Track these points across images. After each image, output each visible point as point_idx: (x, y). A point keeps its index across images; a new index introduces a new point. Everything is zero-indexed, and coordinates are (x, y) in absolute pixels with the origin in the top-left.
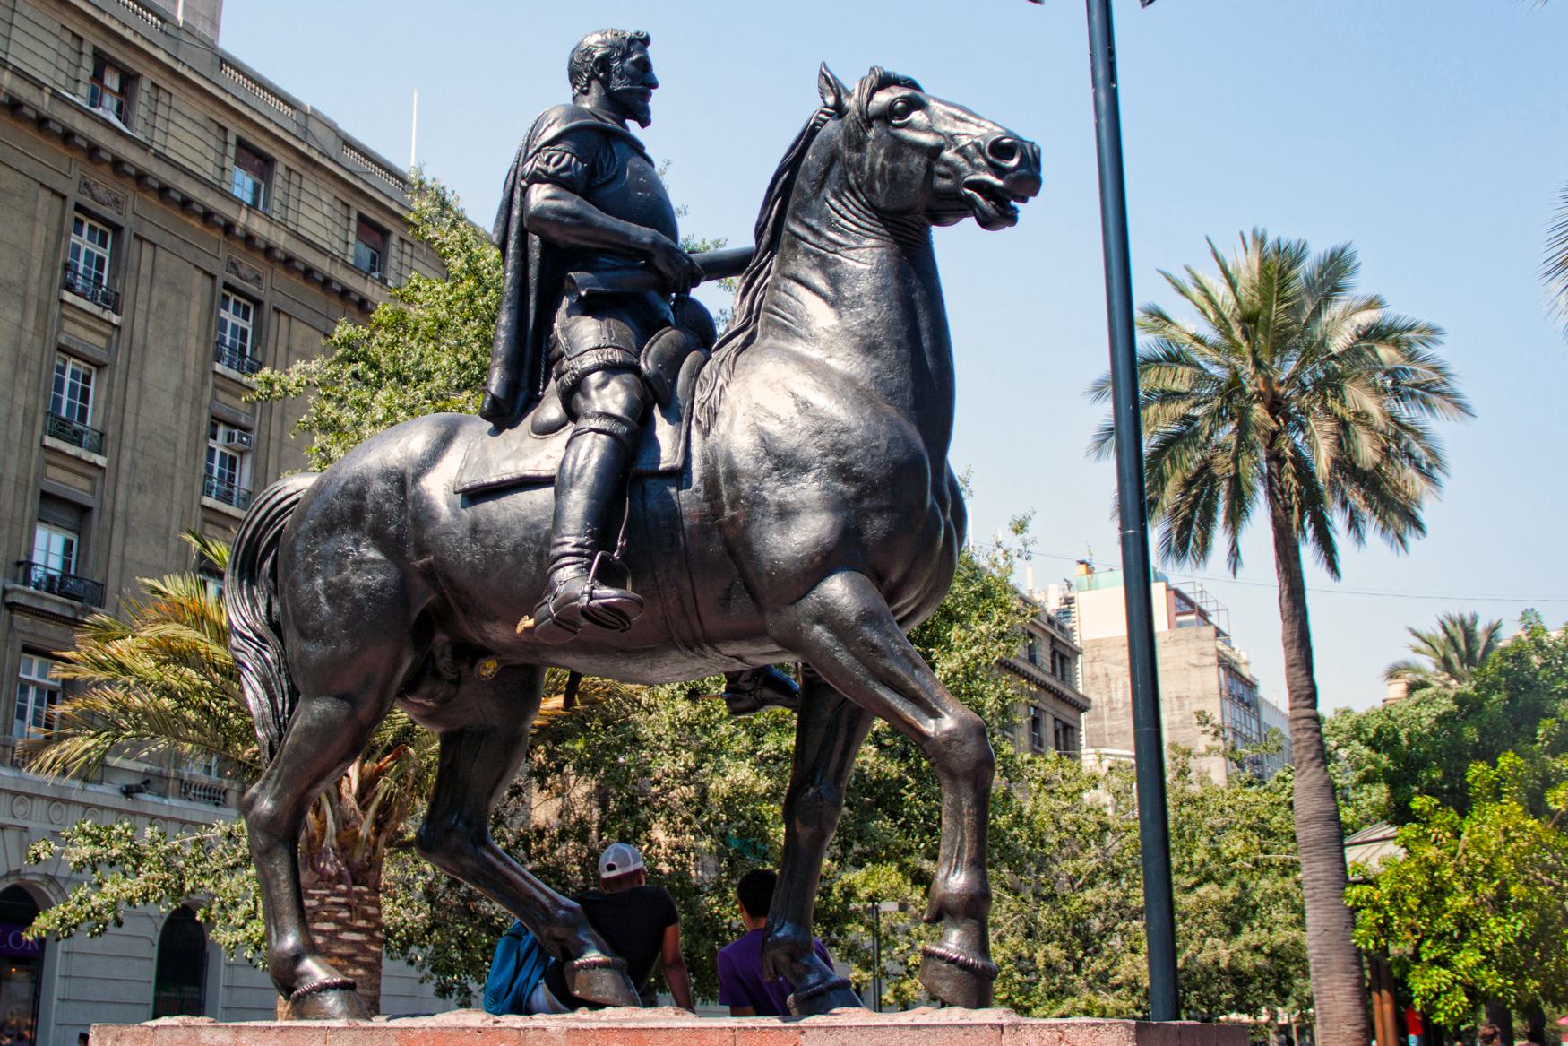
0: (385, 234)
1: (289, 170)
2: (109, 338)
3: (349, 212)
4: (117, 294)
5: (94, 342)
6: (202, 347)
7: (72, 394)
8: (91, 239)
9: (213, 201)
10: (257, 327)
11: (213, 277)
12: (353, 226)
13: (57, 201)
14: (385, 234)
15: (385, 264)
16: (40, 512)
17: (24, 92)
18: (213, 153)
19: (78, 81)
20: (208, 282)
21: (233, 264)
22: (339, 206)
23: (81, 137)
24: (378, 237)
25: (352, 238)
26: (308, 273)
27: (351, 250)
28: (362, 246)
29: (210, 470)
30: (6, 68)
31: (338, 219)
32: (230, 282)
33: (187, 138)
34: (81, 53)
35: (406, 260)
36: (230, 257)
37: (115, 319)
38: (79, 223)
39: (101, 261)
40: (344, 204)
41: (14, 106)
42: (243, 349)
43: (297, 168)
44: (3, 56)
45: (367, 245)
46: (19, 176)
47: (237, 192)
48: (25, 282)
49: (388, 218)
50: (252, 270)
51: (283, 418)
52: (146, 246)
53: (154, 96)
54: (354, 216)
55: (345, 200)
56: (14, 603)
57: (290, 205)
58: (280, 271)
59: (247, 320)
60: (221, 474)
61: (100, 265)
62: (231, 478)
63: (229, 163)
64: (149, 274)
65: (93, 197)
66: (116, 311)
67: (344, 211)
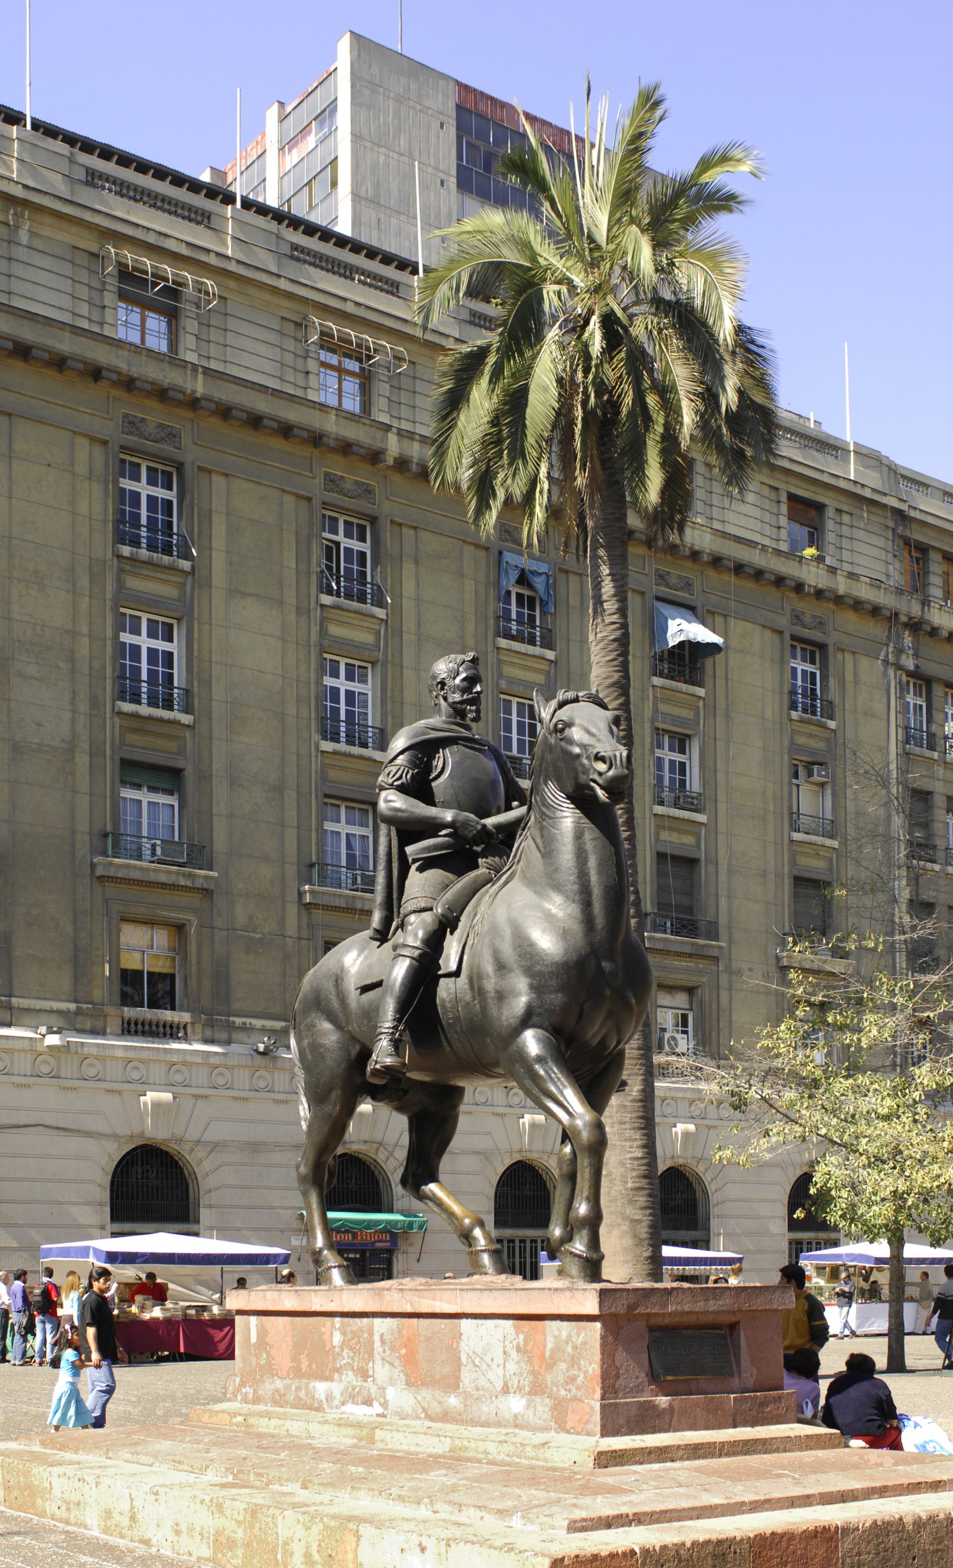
0: (820, 508)
1: (839, 511)
2: (828, 740)
3: (778, 496)
4: (550, 630)
5: (165, 590)
6: (777, 698)
7: (521, 731)
8: (348, 535)
9: (293, 414)
10: (181, 496)
11: (781, 633)
12: (784, 508)
13: (304, 504)
14: (820, 508)
15: (823, 540)
16: (795, 892)
17: (28, 334)
18: (86, 289)
19: (308, 373)
20: (776, 638)
21: (661, 576)
22: (766, 491)
23: (73, 359)
24: (813, 513)
25: (783, 521)
26: (739, 568)
27: (784, 534)
28: (796, 527)
29: (660, 778)
30: (413, 439)
31: (767, 504)
32: (660, 595)
33: (42, 277)
34: (779, 502)
35: (845, 530)
36: (657, 570)
37: (550, 655)
38: (793, 647)
39: (362, 555)
40: (771, 487)
41: (23, 351)
42: (813, 691)
43: (845, 508)
44: (3, 299)
45: (802, 524)
46: (443, 538)
47: (121, 334)
48: (462, 638)
49: (819, 490)
50: (680, 577)
51: (728, 717)
52: (571, 576)
53: (708, 476)
54: (784, 498)
55: (772, 483)
56: (102, 876)
57: (715, 502)
58: (711, 573)
59: (170, 489)
60: (672, 780)
61: (362, 562)
62: (683, 783)
63: (109, 298)
64: (578, 605)
65: (667, 586)
66: (550, 647)
67: (773, 496)
